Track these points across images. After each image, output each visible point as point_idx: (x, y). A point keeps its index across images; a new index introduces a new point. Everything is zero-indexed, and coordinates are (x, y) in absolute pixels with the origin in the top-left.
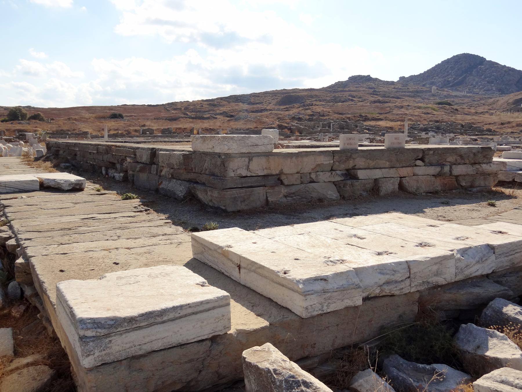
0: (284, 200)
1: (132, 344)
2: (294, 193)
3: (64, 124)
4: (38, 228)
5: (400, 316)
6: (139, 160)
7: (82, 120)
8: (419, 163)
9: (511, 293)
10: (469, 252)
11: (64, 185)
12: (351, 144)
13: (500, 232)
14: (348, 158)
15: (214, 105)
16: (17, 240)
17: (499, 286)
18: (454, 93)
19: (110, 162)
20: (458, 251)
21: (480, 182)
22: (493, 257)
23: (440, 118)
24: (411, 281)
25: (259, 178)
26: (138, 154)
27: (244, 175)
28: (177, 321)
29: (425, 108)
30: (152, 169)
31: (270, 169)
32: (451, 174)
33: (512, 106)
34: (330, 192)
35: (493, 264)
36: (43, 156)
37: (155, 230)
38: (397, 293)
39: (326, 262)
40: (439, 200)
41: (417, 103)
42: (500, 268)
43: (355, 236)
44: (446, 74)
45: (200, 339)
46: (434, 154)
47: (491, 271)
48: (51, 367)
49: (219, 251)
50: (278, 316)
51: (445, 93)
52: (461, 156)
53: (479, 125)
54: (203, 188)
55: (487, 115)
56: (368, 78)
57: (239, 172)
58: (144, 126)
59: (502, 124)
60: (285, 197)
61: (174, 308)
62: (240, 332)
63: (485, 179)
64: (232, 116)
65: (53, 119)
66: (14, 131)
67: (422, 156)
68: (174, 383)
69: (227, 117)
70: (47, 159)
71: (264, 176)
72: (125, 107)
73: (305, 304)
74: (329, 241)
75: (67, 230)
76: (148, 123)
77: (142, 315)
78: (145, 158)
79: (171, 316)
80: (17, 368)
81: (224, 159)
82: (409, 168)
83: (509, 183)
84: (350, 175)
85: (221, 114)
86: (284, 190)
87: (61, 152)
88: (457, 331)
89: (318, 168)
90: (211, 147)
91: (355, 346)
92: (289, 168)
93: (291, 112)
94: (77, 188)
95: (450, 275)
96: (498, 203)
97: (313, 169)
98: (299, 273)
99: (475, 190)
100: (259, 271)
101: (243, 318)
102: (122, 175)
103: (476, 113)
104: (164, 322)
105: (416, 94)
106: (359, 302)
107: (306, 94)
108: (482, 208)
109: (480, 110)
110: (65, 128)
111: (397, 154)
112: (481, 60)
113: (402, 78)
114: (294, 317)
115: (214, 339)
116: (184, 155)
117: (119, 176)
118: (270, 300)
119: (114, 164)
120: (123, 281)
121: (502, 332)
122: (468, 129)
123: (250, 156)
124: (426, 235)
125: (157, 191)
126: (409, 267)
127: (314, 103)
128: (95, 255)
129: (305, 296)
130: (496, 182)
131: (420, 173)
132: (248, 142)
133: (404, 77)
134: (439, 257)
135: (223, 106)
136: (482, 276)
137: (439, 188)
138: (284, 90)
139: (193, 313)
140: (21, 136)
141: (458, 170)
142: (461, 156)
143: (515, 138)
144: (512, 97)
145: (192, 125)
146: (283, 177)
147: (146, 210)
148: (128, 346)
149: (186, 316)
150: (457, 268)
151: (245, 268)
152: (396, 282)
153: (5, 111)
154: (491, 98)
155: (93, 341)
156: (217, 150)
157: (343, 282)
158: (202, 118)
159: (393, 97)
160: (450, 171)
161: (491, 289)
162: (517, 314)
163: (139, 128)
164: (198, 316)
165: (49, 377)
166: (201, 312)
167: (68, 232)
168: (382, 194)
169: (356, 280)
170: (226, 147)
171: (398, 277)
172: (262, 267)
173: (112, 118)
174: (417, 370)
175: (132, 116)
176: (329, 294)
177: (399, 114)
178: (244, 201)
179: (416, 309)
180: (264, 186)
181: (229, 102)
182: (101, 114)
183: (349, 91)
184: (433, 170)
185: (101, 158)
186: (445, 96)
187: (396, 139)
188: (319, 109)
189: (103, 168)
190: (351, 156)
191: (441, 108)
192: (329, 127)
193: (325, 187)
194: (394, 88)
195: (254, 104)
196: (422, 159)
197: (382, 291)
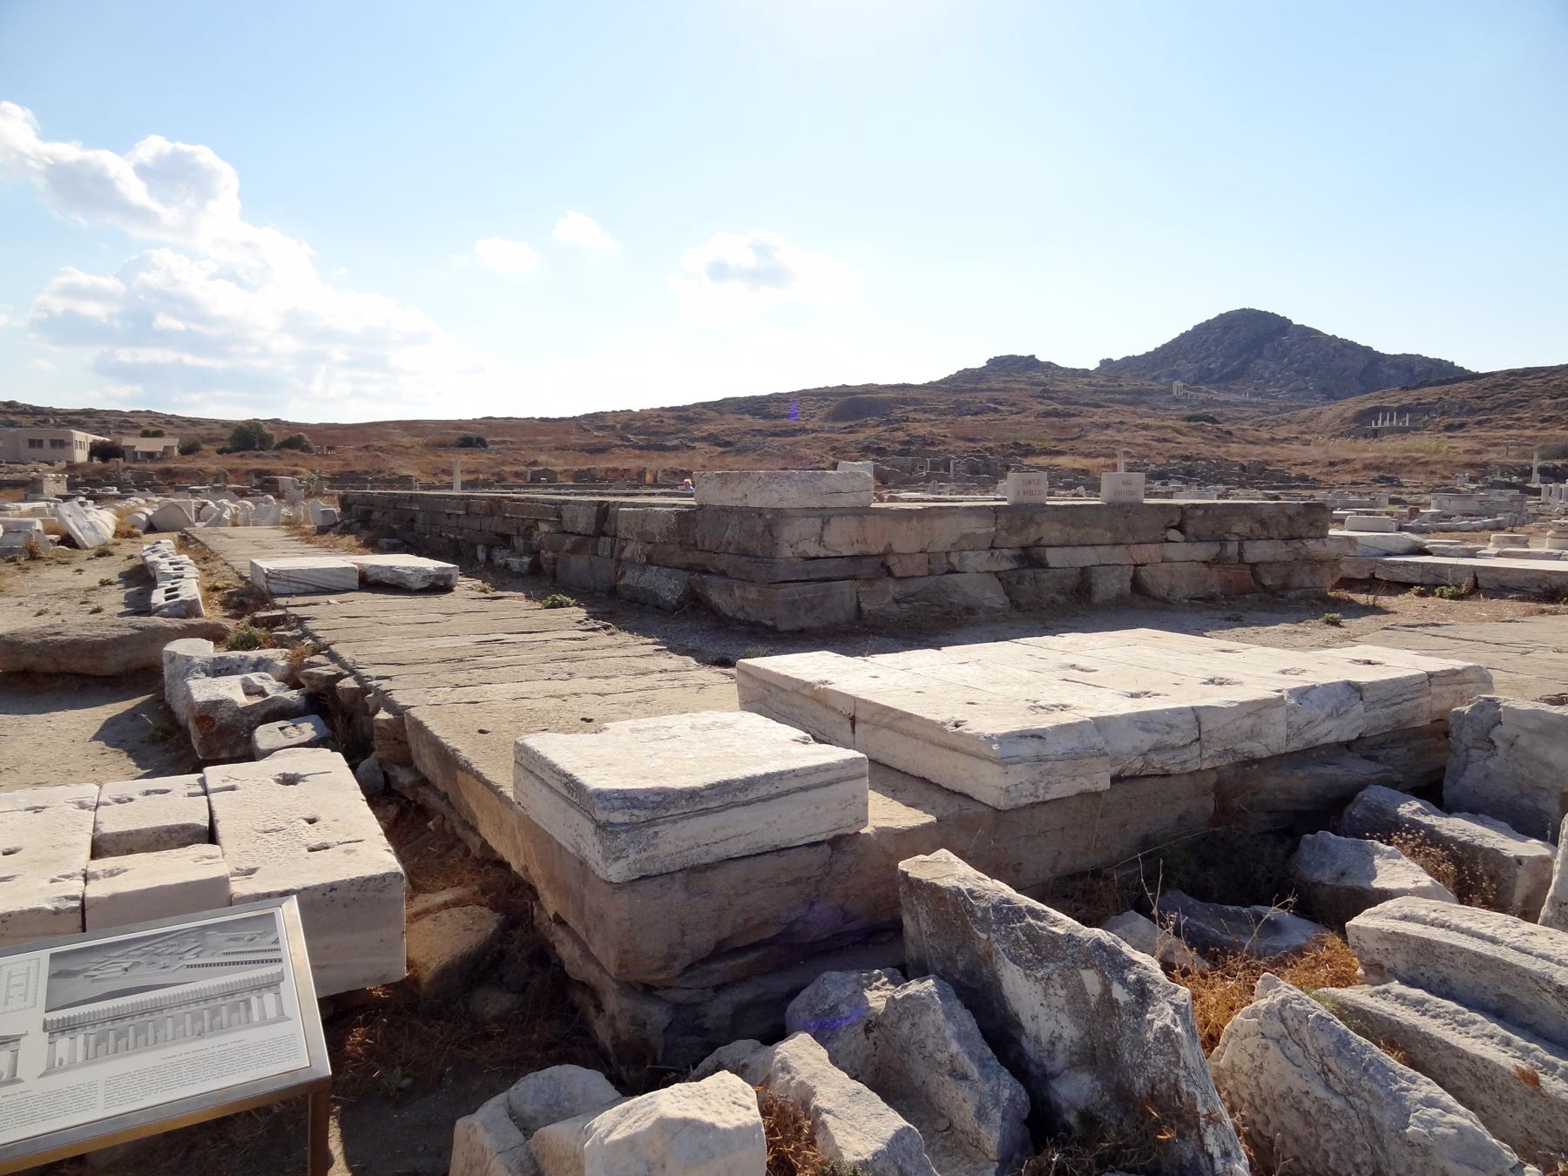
0: (895, 608)
1: (693, 842)
2: (913, 595)
3: (356, 458)
4: (392, 659)
5: (1180, 818)
6: (568, 527)
7: (404, 451)
8: (1173, 534)
9: (1399, 777)
10: (1313, 695)
11: (412, 579)
12: (1031, 493)
13: (1369, 663)
14: (1029, 522)
15: (689, 420)
16: (359, 679)
17: (1373, 764)
18: (1223, 397)
19: (497, 534)
20: (1292, 692)
21: (1303, 578)
22: (1360, 707)
23: (1192, 451)
24: (1202, 747)
25: (844, 562)
26: (566, 515)
27: (812, 554)
28: (776, 801)
29: (1160, 428)
30: (601, 545)
31: (865, 541)
32: (1241, 560)
33: (1353, 426)
34: (989, 594)
35: (1360, 722)
36: (336, 524)
37: (642, 664)
38: (1176, 769)
39: (1032, 708)
40: (1219, 614)
41: (1141, 417)
42: (1374, 729)
43: (1073, 666)
45: (812, 839)
46: (1204, 516)
47: (1354, 736)
48: (495, 908)
49: (806, 692)
50: (953, 808)
51: (1202, 396)
52: (1263, 523)
53: (1280, 466)
54: (722, 581)
55: (1296, 446)
56: (1030, 363)
58: (535, 463)
59: (1332, 464)
60: (897, 601)
61: (768, 777)
62: (881, 832)
63: (1313, 572)
64: (728, 444)
65: (330, 448)
66: (248, 472)
67: (1181, 520)
68: (765, 923)
69: (719, 445)
70: (345, 530)
72: (489, 422)
73: (1004, 782)
74: (1025, 674)
75: (456, 661)
76: (542, 458)
77: (712, 787)
78: (583, 523)
79: (763, 791)
80: (427, 912)
81: (772, 521)
83: (1363, 581)
84: (1030, 558)
85: (704, 439)
86: (894, 588)
87: (376, 515)
88: (1294, 848)
89: (964, 543)
90: (740, 495)
91: (1096, 873)
92: (906, 541)
93: (860, 436)
94: (438, 586)
95: (1275, 739)
96: (1345, 622)
97: (953, 545)
98: (986, 724)
99: (1291, 594)
100: (902, 725)
101: (886, 813)
102: (526, 560)
103: (1273, 439)
105: (1137, 398)
106: (1105, 784)
107: (893, 395)
108: (1316, 629)
109: (1281, 433)
110: (359, 467)
111: (1123, 513)
112: (1284, 324)
113: (1106, 363)
114: (981, 809)
115: (837, 843)
116: (679, 514)
117: (519, 563)
118: (923, 779)
120: (646, 735)
121: (1389, 844)
122: (1255, 475)
123: (825, 516)
124: (1220, 665)
125: (613, 592)
126: (1197, 719)
127: (912, 415)
128: (538, 705)
129: (1005, 765)
130: (1337, 579)
132: (819, 484)
133: (1109, 361)
134: (1256, 702)
135: (708, 421)
136: (1339, 744)
137: (1217, 590)
138: (844, 386)
140: (268, 484)
141: (1258, 551)
142: (1263, 523)
143: (1360, 495)
144: (1350, 406)
145: (641, 463)
146: (892, 561)
147: (606, 628)
148: (686, 845)
149: (788, 793)
150: (1289, 725)
151: (865, 722)
152: (1173, 748)
153: (224, 431)
154: (1304, 408)
155: (627, 831)
156: (755, 502)
157: (1073, 743)
158: (662, 448)
159: (1087, 405)
160: (1240, 554)
161: (1357, 769)
162: (1415, 812)
163: (523, 468)
165: (495, 925)
166: (815, 787)
167: (461, 665)
168: (1096, 599)
169: (1097, 740)
171: (1176, 738)
172: (908, 717)
173: (461, 446)
174: (1227, 916)
175: (504, 442)
176: (1049, 765)
177: (1102, 442)
178: (811, 610)
179: (1210, 804)
180: (854, 578)
181: (721, 414)
182: (438, 438)
183: (990, 389)
184: (1203, 551)
186: (1203, 402)
187: (1124, 483)
188: (922, 430)
189: (480, 548)
190: (1032, 518)
191: (1195, 428)
192: (947, 469)
193: (977, 581)
194: (1090, 384)
195: (776, 417)
196: (1180, 528)
197: (1147, 764)
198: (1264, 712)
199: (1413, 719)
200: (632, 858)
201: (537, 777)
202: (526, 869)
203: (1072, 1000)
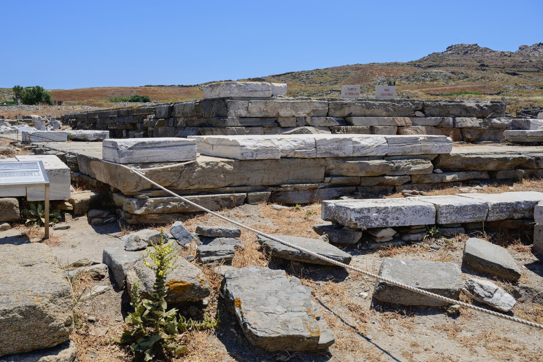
8: (418, 113)
25: (258, 119)
27: (243, 115)
71: (262, 118)
79: (164, 145)
90: (217, 93)
104: (159, 147)
119: (134, 125)
139: (175, 146)
146: (280, 120)
148: (141, 156)
149: (171, 146)
164: (178, 147)
185: (122, 120)
189: (124, 131)
196: (422, 111)
198: (342, 142)
200: (126, 157)
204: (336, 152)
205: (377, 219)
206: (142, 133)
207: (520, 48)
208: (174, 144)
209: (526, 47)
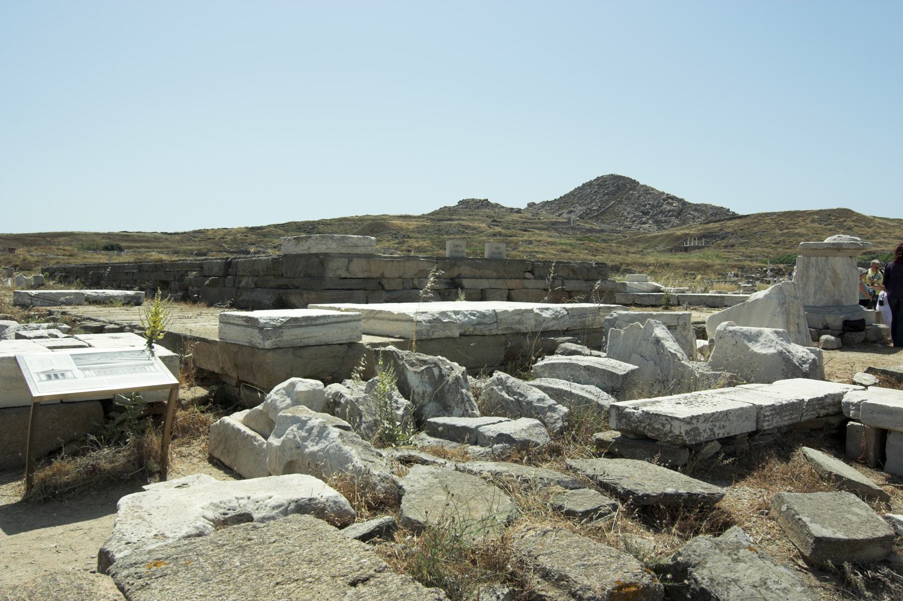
8: (528, 275)
12: (458, 252)
14: (453, 266)
18: (597, 227)
25: (360, 281)
27: (343, 276)
30: (227, 281)
38: (487, 333)
44: (589, 200)
51: (588, 226)
52: (573, 271)
56: (485, 204)
57: (338, 273)
79: (322, 321)
82: (518, 281)
90: (306, 248)
100: (378, 316)
104: (316, 325)
112: (634, 183)
123: (350, 257)
131: (530, 286)
146: (384, 282)
149: (331, 323)
150: (536, 321)
152: (486, 324)
164: (340, 325)
170: (325, 247)
171: (487, 320)
197: (475, 329)
199: (593, 324)
201: (233, 324)
202: (222, 368)
203: (430, 379)
204: (517, 327)
205: (705, 431)
206: (180, 294)
207: (529, 205)
208: (334, 320)
209: (534, 204)
